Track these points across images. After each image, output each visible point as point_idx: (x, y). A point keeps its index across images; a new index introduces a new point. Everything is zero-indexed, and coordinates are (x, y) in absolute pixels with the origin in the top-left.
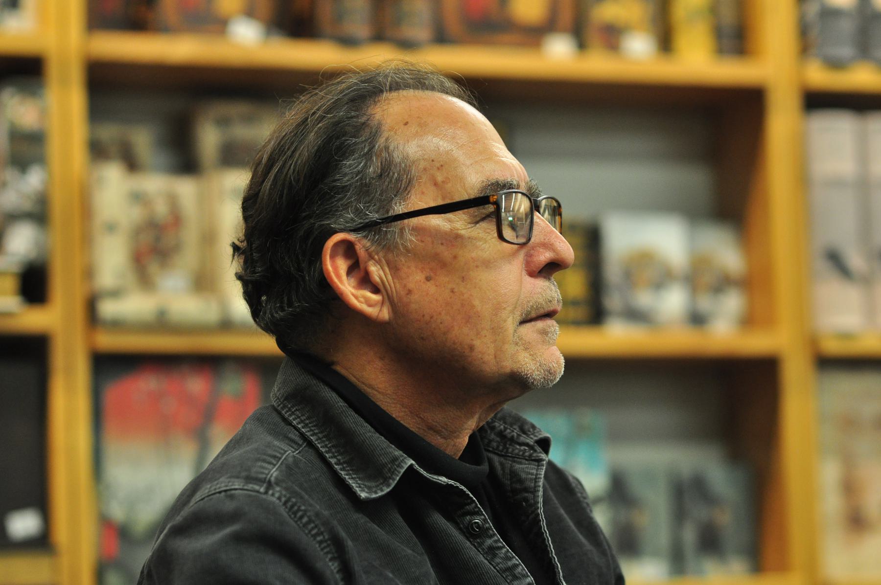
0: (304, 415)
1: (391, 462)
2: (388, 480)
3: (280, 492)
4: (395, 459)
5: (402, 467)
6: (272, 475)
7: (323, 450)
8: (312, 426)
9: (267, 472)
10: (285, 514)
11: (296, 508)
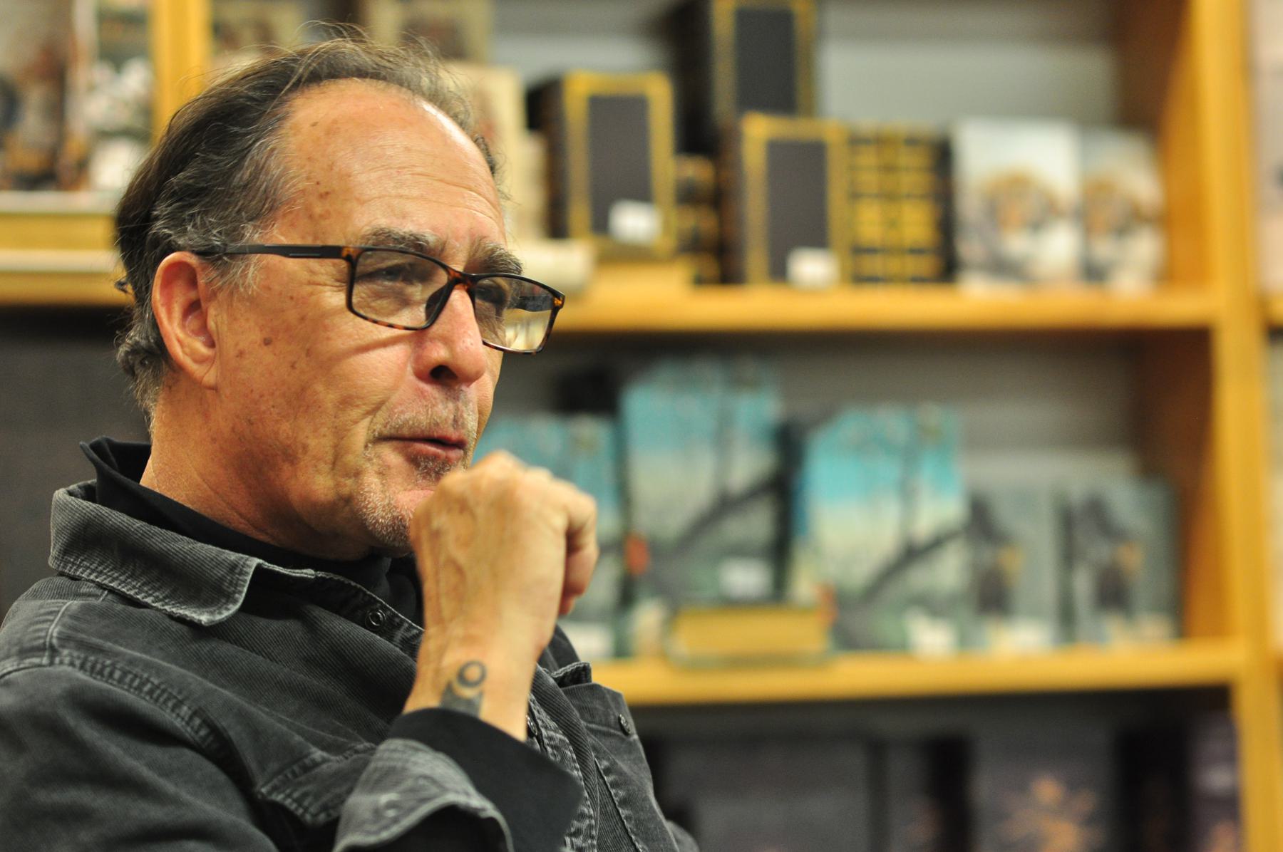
0: (94, 563)
3: (70, 655)
5: (247, 573)
6: (52, 637)
7: (132, 593)
9: (43, 634)
10: (91, 680)
11: (99, 666)
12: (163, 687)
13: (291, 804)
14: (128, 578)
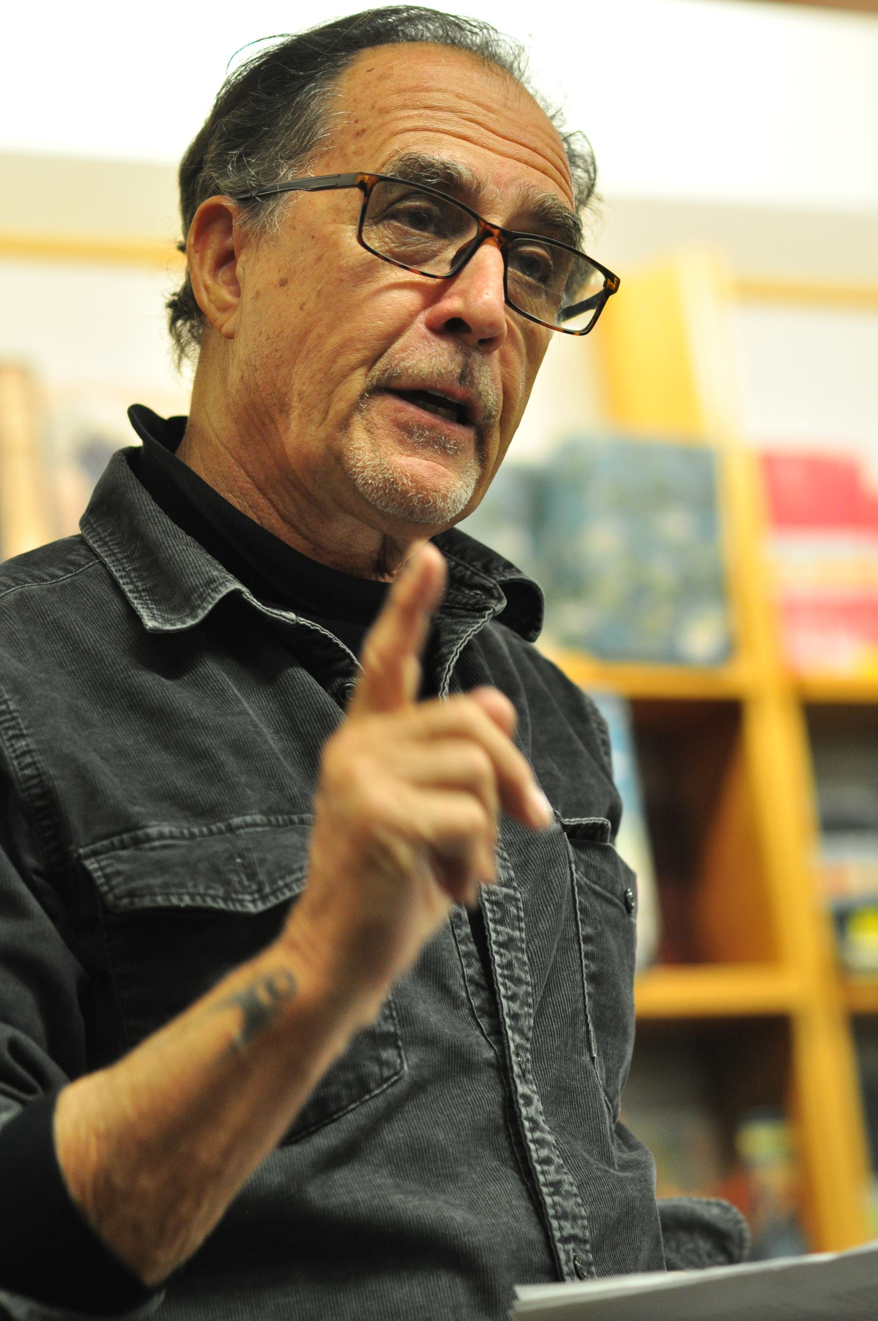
1: (205, 585)
2: (196, 609)
4: (211, 581)
7: (117, 575)
8: (113, 545)
12: (15, 714)
13: (99, 877)
14: (125, 557)
